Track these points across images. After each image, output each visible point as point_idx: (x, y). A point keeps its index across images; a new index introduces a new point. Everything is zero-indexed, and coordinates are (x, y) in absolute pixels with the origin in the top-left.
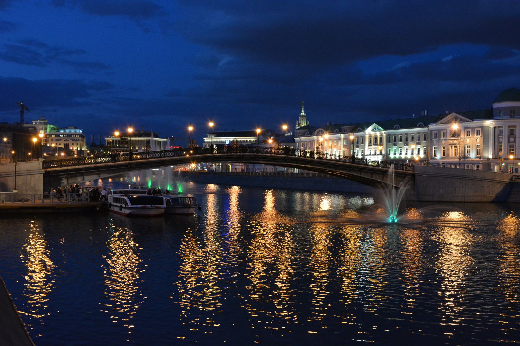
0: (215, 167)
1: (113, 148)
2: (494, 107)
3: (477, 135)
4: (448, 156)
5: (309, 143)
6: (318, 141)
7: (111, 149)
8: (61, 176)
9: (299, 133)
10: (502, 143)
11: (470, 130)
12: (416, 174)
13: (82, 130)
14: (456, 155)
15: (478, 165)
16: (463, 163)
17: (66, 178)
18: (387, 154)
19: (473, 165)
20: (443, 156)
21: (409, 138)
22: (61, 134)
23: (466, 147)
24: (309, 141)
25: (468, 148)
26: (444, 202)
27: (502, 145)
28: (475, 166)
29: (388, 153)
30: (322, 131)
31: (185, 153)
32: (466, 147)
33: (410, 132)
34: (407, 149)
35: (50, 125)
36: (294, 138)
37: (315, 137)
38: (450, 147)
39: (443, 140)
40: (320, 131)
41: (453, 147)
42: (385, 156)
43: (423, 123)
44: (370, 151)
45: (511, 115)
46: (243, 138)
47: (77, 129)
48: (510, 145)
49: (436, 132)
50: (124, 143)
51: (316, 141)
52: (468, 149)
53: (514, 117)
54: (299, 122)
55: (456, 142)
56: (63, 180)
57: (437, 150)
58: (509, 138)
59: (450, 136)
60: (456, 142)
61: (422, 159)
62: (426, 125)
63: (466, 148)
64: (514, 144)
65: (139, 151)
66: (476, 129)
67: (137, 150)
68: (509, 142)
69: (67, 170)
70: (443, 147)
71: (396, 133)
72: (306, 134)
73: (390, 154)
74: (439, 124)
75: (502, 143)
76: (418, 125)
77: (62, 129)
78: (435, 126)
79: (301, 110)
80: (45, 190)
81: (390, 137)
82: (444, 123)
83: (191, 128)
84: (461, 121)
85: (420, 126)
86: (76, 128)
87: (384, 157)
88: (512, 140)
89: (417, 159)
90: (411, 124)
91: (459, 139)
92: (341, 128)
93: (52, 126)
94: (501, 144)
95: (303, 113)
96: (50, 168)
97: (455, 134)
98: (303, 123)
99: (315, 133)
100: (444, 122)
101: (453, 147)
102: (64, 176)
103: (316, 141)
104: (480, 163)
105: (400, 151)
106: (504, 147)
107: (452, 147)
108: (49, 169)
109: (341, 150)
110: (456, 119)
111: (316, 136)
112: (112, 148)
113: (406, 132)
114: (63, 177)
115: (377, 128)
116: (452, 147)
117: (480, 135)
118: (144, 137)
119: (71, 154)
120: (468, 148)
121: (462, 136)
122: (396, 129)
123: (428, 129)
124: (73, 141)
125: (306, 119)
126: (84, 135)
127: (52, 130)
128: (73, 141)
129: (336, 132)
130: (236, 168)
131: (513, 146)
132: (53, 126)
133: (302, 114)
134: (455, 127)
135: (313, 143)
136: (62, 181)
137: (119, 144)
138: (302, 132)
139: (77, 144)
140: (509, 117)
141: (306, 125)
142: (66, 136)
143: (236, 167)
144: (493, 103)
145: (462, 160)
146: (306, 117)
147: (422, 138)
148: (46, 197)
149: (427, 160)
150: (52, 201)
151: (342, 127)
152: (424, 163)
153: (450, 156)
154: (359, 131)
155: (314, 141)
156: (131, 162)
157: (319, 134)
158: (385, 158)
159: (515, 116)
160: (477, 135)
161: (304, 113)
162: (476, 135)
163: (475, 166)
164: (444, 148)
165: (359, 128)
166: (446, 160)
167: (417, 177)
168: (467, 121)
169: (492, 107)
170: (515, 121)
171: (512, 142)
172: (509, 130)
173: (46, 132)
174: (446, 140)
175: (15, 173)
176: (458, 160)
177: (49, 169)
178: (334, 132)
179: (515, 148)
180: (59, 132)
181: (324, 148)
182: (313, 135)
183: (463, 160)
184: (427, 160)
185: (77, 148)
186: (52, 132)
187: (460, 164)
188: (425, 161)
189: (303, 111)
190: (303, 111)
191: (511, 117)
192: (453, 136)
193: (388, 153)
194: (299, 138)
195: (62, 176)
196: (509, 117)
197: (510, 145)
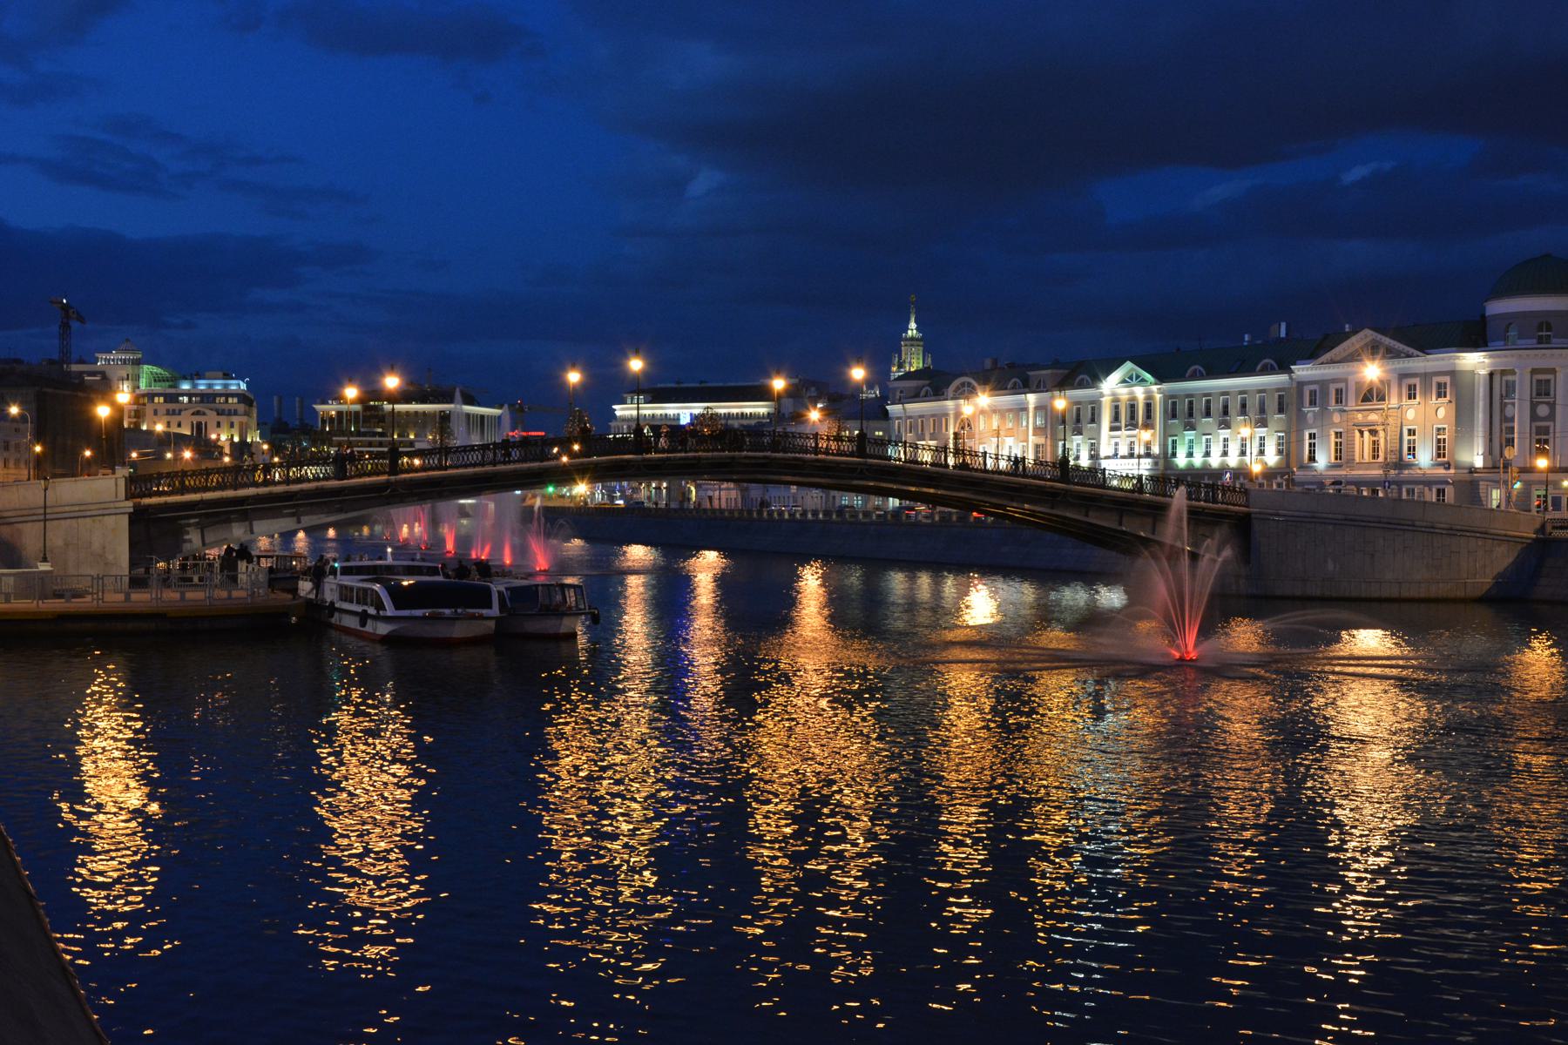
0: (647, 493)
3: (1439, 396)
6: (958, 414)
8: (183, 522)
9: (901, 392)
10: (1512, 419)
11: (1417, 381)
12: (1253, 516)
13: (247, 383)
15: (1441, 487)
19: (1426, 489)
20: (1336, 459)
21: (1234, 407)
22: (183, 395)
23: (1405, 432)
24: (933, 416)
25: (1409, 435)
27: (1513, 428)
28: (1430, 490)
29: (1170, 451)
30: (969, 384)
31: (558, 452)
32: (1405, 432)
34: (1226, 440)
36: (888, 407)
37: (950, 404)
40: (963, 384)
41: (1366, 434)
42: (1161, 462)
44: (1116, 444)
51: (952, 416)
52: (1412, 438)
53: (1549, 343)
55: (1373, 417)
56: (188, 533)
57: (1316, 441)
58: (1534, 406)
59: (1356, 401)
60: (1373, 417)
62: (1284, 367)
63: (1406, 437)
64: (1551, 424)
65: (418, 446)
66: (1436, 379)
67: (411, 444)
68: (1534, 417)
72: (923, 393)
73: (1174, 455)
75: (1514, 422)
76: (1259, 367)
77: (185, 378)
78: (1312, 369)
79: (908, 322)
80: (133, 564)
83: (574, 377)
84: (1391, 354)
85: (1266, 371)
86: (227, 376)
87: (1156, 464)
93: (156, 370)
94: (1510, 425)
95: (913, 329)
96: (150, 496)
97: (1371, 395)
100: (1338, 359)
101: (1366, 434)
102: (192, 521)
103: (952, 416)
104: (1448, 483)
106: (1519, 433)
107: (1362, 433)
108: (146, 501)
109: (1027, 441)
110: (1374, 350)
111: (952, 399)
112: (336, 436)
113: (1225, 387)
115: (1138, 377)
116: (1362, 433)
117: (1448, 398)
118: (431, 403)
120: (1409, 435)
122: (1194, 377)
123: (1291, 378)
124: (218, 414)
125: (921, 348)
127: (155, 381)
128: (218, 414)
131: (1546, 431)
133: (910, 332)
134: (1372, 371)
136: (187, 537)
137: (356, 423)
140: (1535, 341)
143: (710, 493)
145: (1392, 472)
146: (922, 343)
147: (1272, 404)
148: (137, 583)
149: (1288, 473)
150: (154, 596)
151: (1030, 373)
152: (1279, 480)
153: (1357, 460)
155: (946, 415)
156: (393, 478)
157: (962, 393)
158: (1161, 466)
159: (1554, 340)
160: (1439, 396)
161: (915, 332)
162: (1434, 397)
163: (1430, 490)
164: (1338, 435)
166: (1344, 473)
167: (1257, 526)
168: (1408, 356)
174: (1345, 411)
176: (1381, 472)
177: (146, 501)
178: (1006, 389)
179: (1552, 435)
181: (977, 436)
182: (942, 397)
183: (1397, 472)
185: (232, 436)
186: (157, 388)
188: (1282, 475)
189: (913, 325)
190: (913, 325)
191: (1539, 343)
193: (1170, 451)
194: (900, 406)
195: (186, 521)
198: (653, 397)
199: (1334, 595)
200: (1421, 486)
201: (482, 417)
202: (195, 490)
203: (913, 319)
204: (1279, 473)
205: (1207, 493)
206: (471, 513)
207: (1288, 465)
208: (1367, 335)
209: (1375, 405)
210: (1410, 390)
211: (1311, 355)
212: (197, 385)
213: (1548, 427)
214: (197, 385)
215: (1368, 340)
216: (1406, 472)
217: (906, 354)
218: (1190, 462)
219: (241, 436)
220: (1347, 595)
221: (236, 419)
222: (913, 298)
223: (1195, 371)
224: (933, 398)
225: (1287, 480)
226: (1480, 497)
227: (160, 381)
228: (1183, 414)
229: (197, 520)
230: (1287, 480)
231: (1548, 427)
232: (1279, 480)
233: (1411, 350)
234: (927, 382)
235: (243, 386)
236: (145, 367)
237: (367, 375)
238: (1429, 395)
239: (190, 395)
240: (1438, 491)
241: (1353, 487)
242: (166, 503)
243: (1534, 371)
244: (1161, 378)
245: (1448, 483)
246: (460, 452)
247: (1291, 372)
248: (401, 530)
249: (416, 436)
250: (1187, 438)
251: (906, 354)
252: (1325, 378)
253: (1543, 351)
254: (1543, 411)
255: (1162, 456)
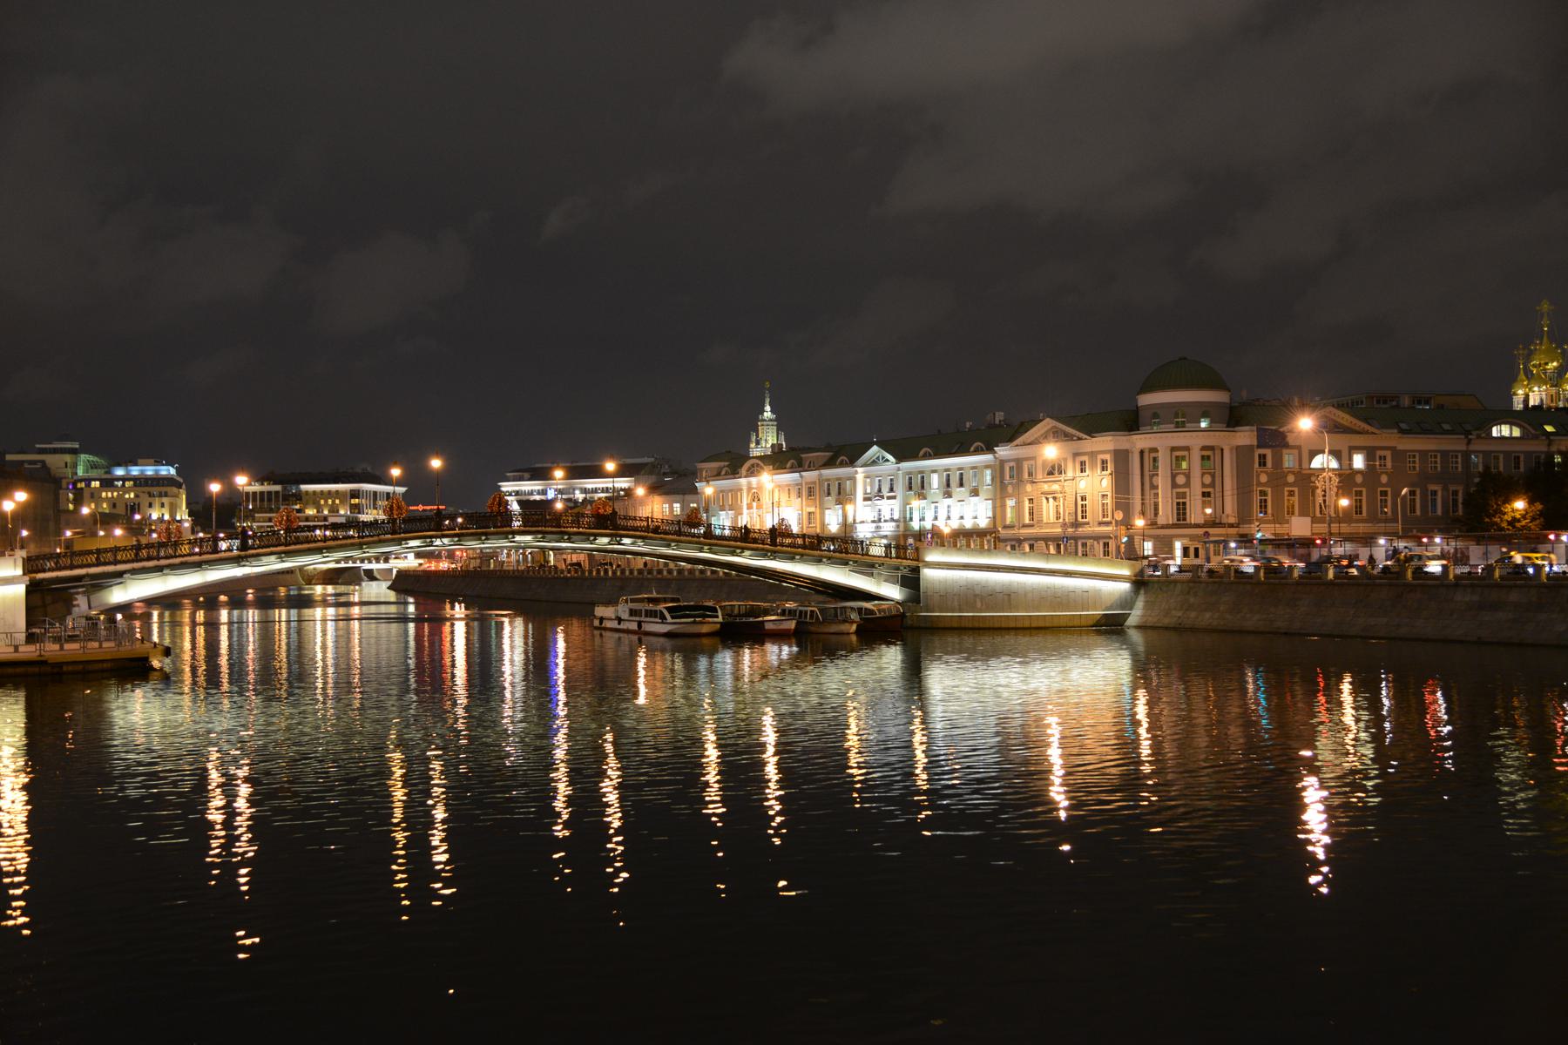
1: (262, 512)
2: (1139, 405)
3: (1103, 469)
4: (1040, 521)
5: (730, 494)
6: (750, 488)
7: (256, 515)
8: (72, 591)
9: (707, 471)
10: (1157, 487)
11: (1085, 458)
13: (176, 468)
14: (1058, 518)
15: (1106, 541)
16: (1072, 538)
17: (83, 593)
18: (905, 518)
19: (1096, 542)
21: (955, 480)
22: (118, 480)
23: (1079, 499)
24: (731, 491)
25: (1082, 500)
26: (989, 629)
27: (1158, 494)
28: (1098, 543)
29: (908, 516)
30: (758, 465)
32: (1079, 499)
33: (956, 464)
34: (949, 507)
35: (87, 456)
37: (743, 481)
38: (1044, 501)
39: (1009, 483)
40: (753, 466)
41: (1051, 500)
42: (902, 525)
43: (983, 443)
44: (936, 507)
45: (1177, 422)
46: (599, 483)
47: (163, 465)
48: (1177, 493)
49: (1012, 464)
50: (291, 499)
52: (1084, 503)
54: (757, 435)
55: (1056, 487)
56: (76, 599)
58: (1173, 477)
59: (1043, 474)
60: (1056, 487)
61: (955, 530)
62: (989, 448)
63: (1080, 503)
64: (1187, 490)
65: (332, 520)
66: (1100, 457)
67: (325, 519)
68: (1174, 485)
69: (87, 575)
70: (1030, 500)
71: (923, 467)
72: (723, 473)
73: (911, 519)
74: (1017, 446)
75: (1158, 489)
76: (972, 449)
77: (119, 465)
78: (1009, 450)
79: (764, 406)
80: (29, 624)
81: (910, 479)
82: (1029, 444)
83: (436, 463)
84: (1068, 437)
85: (978, 451)
86: (158, 463)
87: (898, 526)
88: (1181, 480)
89: (946, 531)
90: (958, 446)
91: (1060, 481)
92: (801, 458)
93: (91, 458)
94: (1155, 491)
95: (768, 414)
96: (44, 571)
97: (1054, 470)
98: (770, 439)
99: (743, 471)
100: (1029, 441)
101: (1051, 500)
102: (80, 590)
104: (1111, 538)
105: (936, 512)
106: (1163, 497)
108: (41, 576)
110: (1057, 435)
111: (745, 477)
112: (258, 513)
113: (947, 465)
114: (78, 593)
115: (883, 458)
116: (1047, 499)
117: (1109, 471)
118: (343, 483)
119: (144, 530)
120: (1082, 500)
121: (1070, 474)
122: (927, 457)
123: (995, 457)
124: (150, 496)
125: (775, 428)
126: (181, 480)
127: (92, 468)
128: (150, 496)
129: (791, 468)
130: (565, 560)
131: (1183, 495)
132: (95, 459)
133: (765, 414)
134: (1051, 452)
135: (739, 494)
136: (75, 603)
138: (714, 468)
139: (163, 505)
141: (775, 442)
142: (132, 483)
143: (565, 556)
144: (1138, 394)
145: (1070, 530)
146: (775, 423)
148: (31, 638)
149: (995, 532)
150: (38, 648)
151: (803, 456)
152: (989, 537)
153: (1045, 521)
154: (842, 465)
155: (741, 490)
157: (752, 473)
158: (902, 529)
160: (1103, 469)
161: (770, 413)
162: (1099, 471)
163: (1098, 543)
164: (1031, 500)
165: (842, 458)
166: (1036, 531)
168: (1079, 439)
169: (1137, 402)
170: (1167, 437)
171: (1180, 487)
172: (1174, 457)
173: (76, 474)
174: (1034, 482)
175: (597, 633)
176: (1060, 530)
177: (41, 576)
178: (785, 468)
179: (1188, 498)
180: (109, 472)
181: (764, 507)
182: (737, 476)
183: (1074, 530)
184: (995, 532)
185: (163, 515)
186: (93, 473)
187: (1065, 539)
188: (991, 533)
189: (768, 408)
190: (768, 408)
192: (1051, 473)
193: (908, 516)
195: (75, 590)
196: (1172, 426)
197: (1177, 493)
198: (531, 475)
199: (981, 626)
200: (1092, 541)
201: (375, 493)
202: (109, 563)
203: (768, 400)
204: (988, 532)
205: (897, 553)
206: (378, 577)
207: (995, 526)
208: (1047, 424)
209: (1056, 477)
210: (1081, 465)
211: (1009, 439)
212: (131, 470)
213: (1185, 493)
214: (131, 470)
215: (1049, 427)
216: (1080, 529)
217: (763, 433)
218: (975, 522)
219: (171, 516)
220: (991, 625)
221: (165, 500)
222: (767, 385)
223: (842, 461)
224: (732, 476)
225: (995, 537)
226: (1135, 548)
227: (96, 468)
228: (918, 487)
229: (84, 589)
230: (995, 537)
231: (1185, 493)
232: (989, 537)
233: (1085, 436)
234: (727, 463)
235: (173, 471)
236: (83, 456)
237: (225, 476)
238: (1095, 469)
239: (124, 479)
240: (1104, 543)
241: (1042, 542)
242: (57, 577)
243: (1173, 449)
244: (900, 458)
245: (1111, 538)
246: (127, 550)
247: (995, 452)
248: (294, 595)
249: (329, 511)
250: (972, 503)
251: (763, 433)
252: (1020, 457)
253: (1178, 434)
254: (1181, 480)
255: (902, 520)
